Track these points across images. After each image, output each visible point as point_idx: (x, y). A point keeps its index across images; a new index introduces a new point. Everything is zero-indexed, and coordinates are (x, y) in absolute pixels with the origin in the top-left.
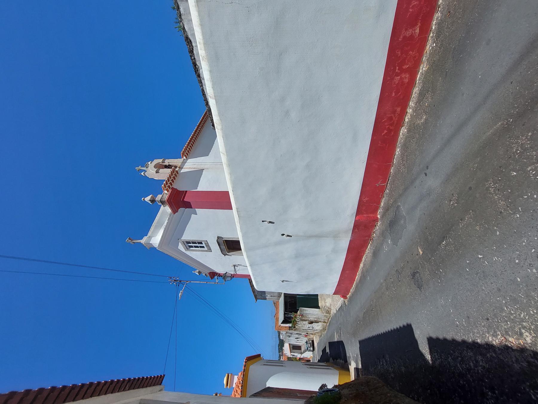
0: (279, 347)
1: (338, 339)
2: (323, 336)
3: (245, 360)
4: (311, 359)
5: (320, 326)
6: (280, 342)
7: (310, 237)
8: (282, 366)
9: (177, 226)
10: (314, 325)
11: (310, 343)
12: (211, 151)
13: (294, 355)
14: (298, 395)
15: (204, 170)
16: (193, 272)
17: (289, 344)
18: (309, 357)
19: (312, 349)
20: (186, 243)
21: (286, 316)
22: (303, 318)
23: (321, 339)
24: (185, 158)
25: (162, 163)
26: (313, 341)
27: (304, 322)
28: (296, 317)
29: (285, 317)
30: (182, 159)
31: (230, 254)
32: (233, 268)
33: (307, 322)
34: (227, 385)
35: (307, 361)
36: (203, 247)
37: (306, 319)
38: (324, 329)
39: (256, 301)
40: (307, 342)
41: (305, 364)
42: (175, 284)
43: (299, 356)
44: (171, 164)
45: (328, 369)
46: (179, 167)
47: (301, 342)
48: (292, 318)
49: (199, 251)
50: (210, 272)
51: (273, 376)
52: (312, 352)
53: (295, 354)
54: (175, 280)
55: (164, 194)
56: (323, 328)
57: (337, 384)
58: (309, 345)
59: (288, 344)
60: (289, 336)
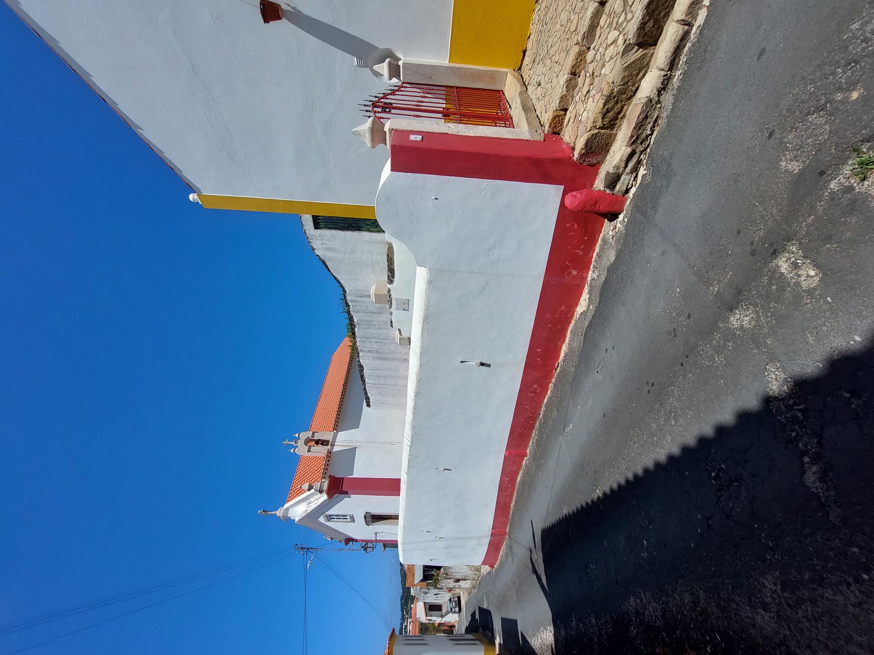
0: (401, 602)
1: (487, 607)
2: (472, 594)
3: (388, 642)
4: (456, 624)
5: (469, 584)
6: (404, 592)
7: (458, 539)
8: (426, 644)
10: (462, 583)
13: (431, 620)
16: (324, 537)
17: (424, 603)
18: (453, 621)
19: (457, 609)
20: (328, 517)
21: (426, 573)
22: (447, 577)
23: (470, 599)
25: (312, 437)
26: (459, 598)
27: (449, 581)
28: (438, 575)
29: (424, 576)
31: (374, 524)
32: (374, 535)
33: (452, 580)
35: (449, 629)
36: (347, 519)
37: (451, 577)
38: (474, 587)
39: (385, 549)
40: (450, 600)
41: (450, 639)
43: (437, 620)
45: (475, 644)
47: (442, 599)
48: (434, 576)
49: (341, 521)
50: (346, 539)
52: (457, 614)
53: (433, 618)
54: (302, 548)
56: (473, 586)
60: (426, 593)
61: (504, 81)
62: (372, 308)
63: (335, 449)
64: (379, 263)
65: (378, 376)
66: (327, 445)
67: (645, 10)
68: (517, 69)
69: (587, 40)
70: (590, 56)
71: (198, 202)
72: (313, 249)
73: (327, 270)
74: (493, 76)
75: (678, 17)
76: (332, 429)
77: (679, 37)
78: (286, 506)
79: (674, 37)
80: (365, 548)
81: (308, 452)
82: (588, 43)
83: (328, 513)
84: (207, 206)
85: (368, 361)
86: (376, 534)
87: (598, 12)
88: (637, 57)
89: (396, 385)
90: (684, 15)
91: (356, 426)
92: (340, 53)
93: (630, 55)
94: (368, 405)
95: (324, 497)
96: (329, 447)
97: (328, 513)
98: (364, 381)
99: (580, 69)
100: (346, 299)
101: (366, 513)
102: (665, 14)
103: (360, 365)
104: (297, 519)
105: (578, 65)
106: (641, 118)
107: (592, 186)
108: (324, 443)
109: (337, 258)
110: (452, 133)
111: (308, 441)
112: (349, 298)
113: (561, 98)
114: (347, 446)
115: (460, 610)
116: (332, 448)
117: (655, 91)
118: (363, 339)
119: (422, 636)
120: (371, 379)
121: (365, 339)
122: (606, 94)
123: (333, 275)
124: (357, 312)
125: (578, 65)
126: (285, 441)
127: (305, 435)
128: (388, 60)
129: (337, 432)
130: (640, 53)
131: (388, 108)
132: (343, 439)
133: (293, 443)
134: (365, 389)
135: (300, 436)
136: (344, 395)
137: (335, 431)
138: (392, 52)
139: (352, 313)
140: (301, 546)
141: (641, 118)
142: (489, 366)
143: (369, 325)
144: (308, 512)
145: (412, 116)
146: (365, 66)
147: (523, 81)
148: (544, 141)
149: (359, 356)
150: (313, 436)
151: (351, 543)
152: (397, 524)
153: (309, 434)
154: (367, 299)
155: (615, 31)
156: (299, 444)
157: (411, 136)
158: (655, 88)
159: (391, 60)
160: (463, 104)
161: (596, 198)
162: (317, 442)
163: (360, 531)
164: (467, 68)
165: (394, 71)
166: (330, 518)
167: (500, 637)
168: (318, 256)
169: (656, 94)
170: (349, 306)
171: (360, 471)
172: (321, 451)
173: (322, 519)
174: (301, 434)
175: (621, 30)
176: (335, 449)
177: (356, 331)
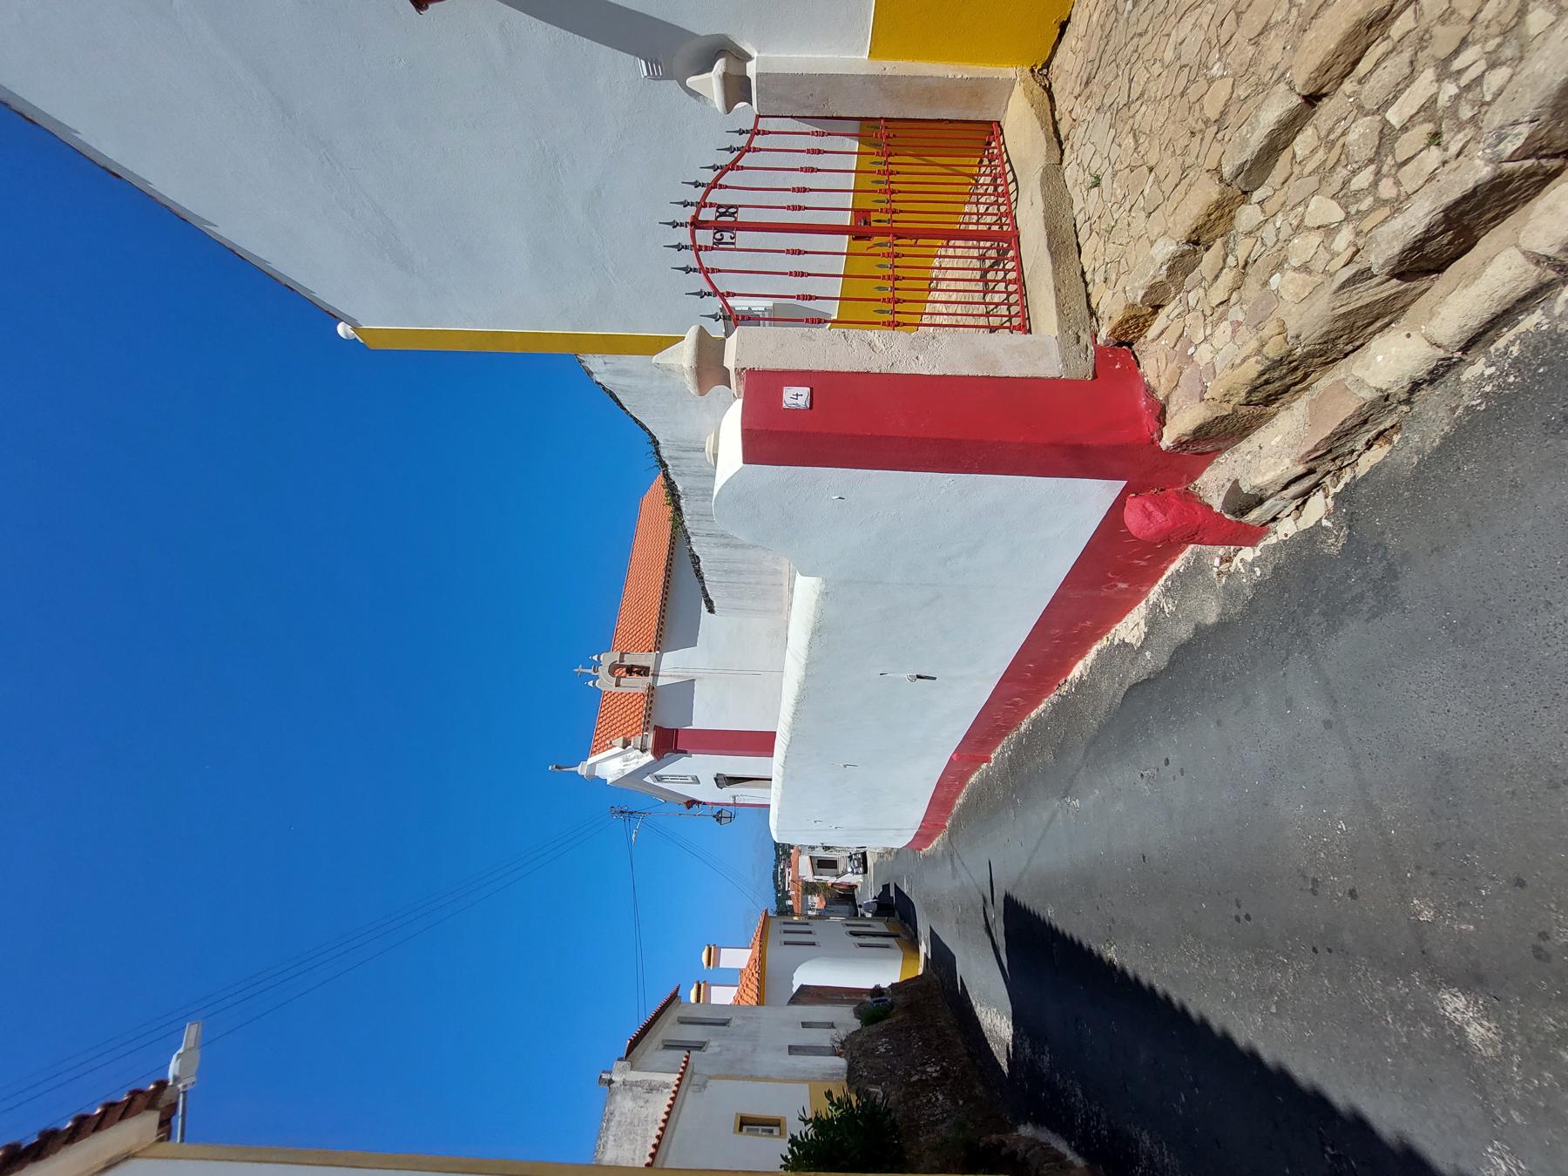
11: (858, 860)
14: (845, 998)
25: (620, 661)
34: (709, 964)
45: (887, 947)
49: (678, 783)
51: (805, 964)
54: (622, 812)
57: (897, 980)
58: (856, 862)
59: (808, 857)
61: (1005, 100)
62: (709, 469)
63: (661, 682)
64: (719, 394)
65: (725, 571)
66: (646, 674)
67: (1442, 214)
68: (1039, 67)
69: (1246, 178)
70: (1248, 215)
71: (356, 339)
72: (590, 373)
73: (618, 407)
74: (977, 90)
75: (1535, 244)
76: (652, 647)
77: (1520, 293)
78: (591, 760)
79: (1502, 291)
80: (719, 818)
81: (616, 686)
82: (1247, 184)
83: (657, 773)
84: (375, 345)
85: (705, 549)
86: (734, 797)
87: (1295, 119)
88: (1376, 298)
89: (757, 583)
90: (1557, 248)
91: (691, 641)
92: (604, 53)
93: (1361, 289)
94: (711, 610)
95: (648, 757)
96: (650, 677)
97: (657, 773)
98: (702, 578)
99: (1213, 234)
100: (659, 455)
101: (718, 775)
102: (1498, 214)
103: (694, 555)
104: (609, 781)
105: (1208, 226)
106: (1348, 423)
107: (1192, 479)
108: (643, 671)
109: (636, 386)
110: (878, 371)
111: (613, 669)
112: (664, 453)
113: (1152, 287)
114: (679, 676)
115: (865, 871)
116: (655, 681)
117: (1406, 383)
118: (696, 517)
119: (807, 924)
120: (714, 575)
121: (700, 518)
122: (1271, 355)
123: (632, 416)
124: (682, 474)
125: (1208, 226)
126: (578, 668)
127: (608, 659)
128: (720, 66)
129: (662, 654)
130: (1392, 288)
131: (726, 224)
132: (673, 666)
133: (591, 671)
134: (704, 588)
135: (601, 659)
136: (671, 560)
137: (658, 652)
138: (730, 40)
139: (673, 477)
140: (618, 809)
141: (1348, 423)
142: (935, 679)
143: (706, 495)
144: (627, 772)
145: (783, 252)
146: (668, 76)
147: (1053, 116)
148: (1095, 376)
149: (690, 541)
150: (622, 660)
151: (695, 806)
152: (770, 787)
153: (615, 657)
154: (698, 455)
155: (1334, 203)
156: (600, 674)
157: (785, 389)
158: (1406, 378)
159: (727, 65)
160: (898, 133)
161: (1199, 527)
162: (630, 670)
163: (707, 792)
164: (915, 77)
165: (737, 89)
166: (660, 779)
167: (927, 945)
168: (599, 383)
169: (1406, 389)
170: (666, 466)
171: (704, 718)
172: (638, 684)
173: (648, 779)
174: (602, 656)
175: (1353, 210)
176: (661, 682)
177: (681, 505)
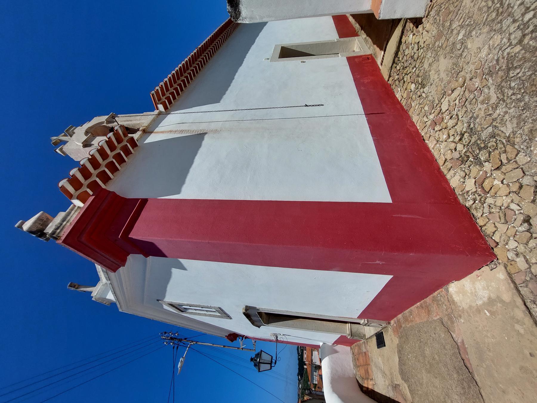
9: (144, 280)
12: (228, 92)
15: (206, 137)
24: (161, 107)
30: (156, 112)
42: (171, 344)
44: (129, 125)
46: (144, 131)
55: (72, 210)
